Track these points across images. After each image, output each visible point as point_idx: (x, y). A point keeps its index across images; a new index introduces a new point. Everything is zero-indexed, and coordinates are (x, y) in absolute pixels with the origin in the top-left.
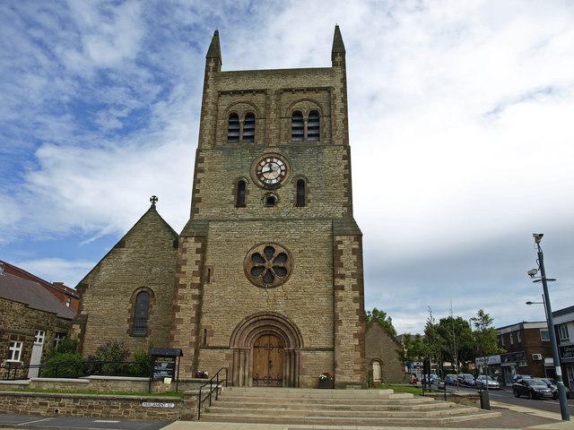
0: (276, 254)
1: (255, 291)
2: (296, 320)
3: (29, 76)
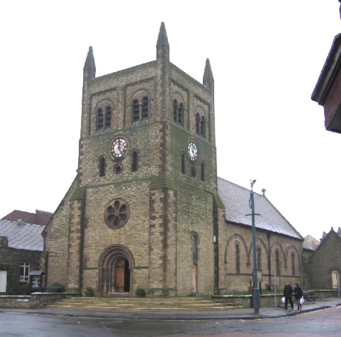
0: (120, 206)
1: (110, 231)
2: (131, 248)
3: (19, 246)
